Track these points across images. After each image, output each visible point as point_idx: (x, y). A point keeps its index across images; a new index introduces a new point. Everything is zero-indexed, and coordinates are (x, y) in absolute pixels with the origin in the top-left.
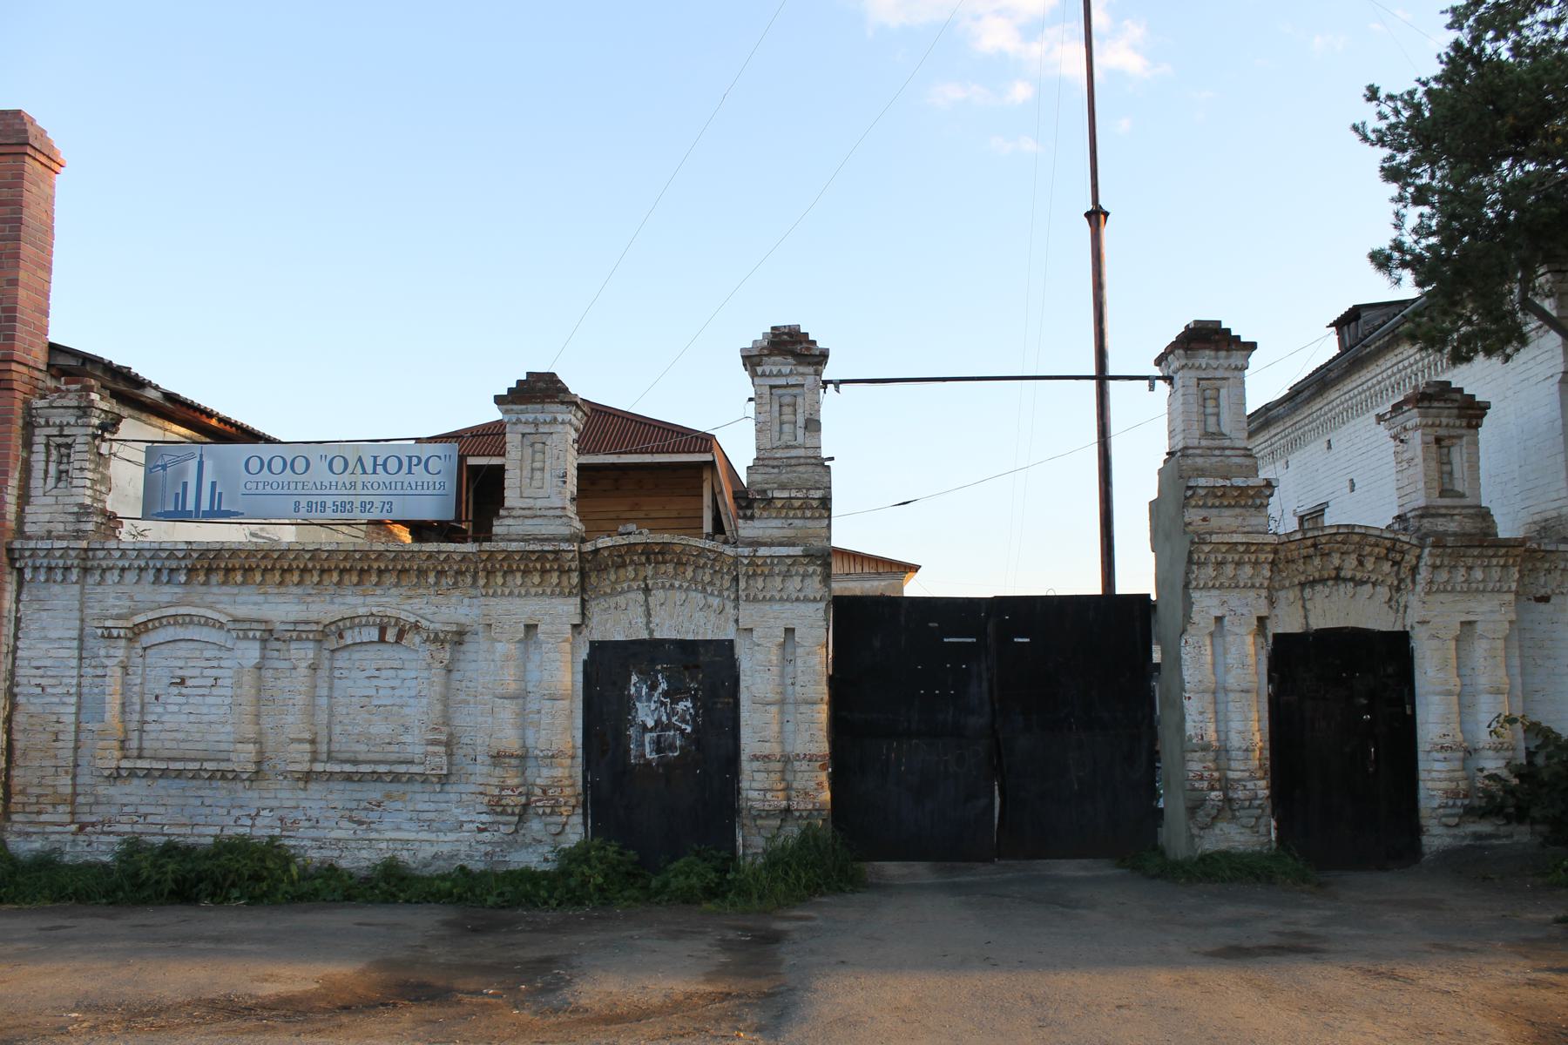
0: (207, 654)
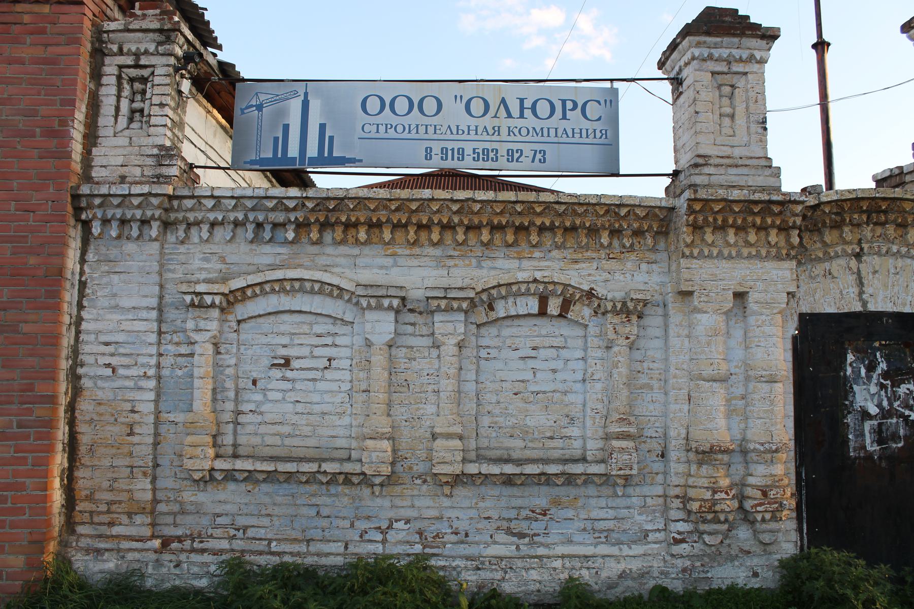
0: (318, 329)
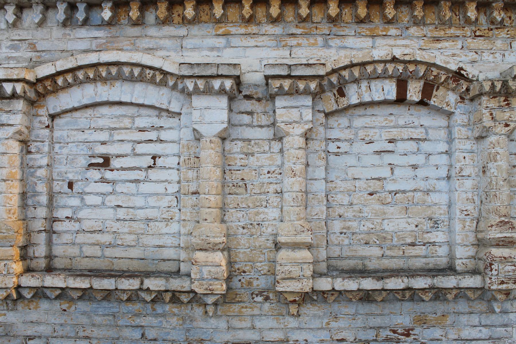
0: (141, 122)
